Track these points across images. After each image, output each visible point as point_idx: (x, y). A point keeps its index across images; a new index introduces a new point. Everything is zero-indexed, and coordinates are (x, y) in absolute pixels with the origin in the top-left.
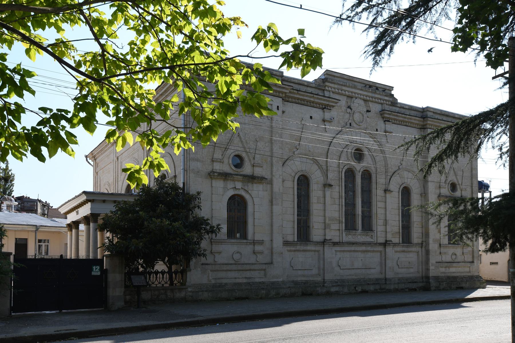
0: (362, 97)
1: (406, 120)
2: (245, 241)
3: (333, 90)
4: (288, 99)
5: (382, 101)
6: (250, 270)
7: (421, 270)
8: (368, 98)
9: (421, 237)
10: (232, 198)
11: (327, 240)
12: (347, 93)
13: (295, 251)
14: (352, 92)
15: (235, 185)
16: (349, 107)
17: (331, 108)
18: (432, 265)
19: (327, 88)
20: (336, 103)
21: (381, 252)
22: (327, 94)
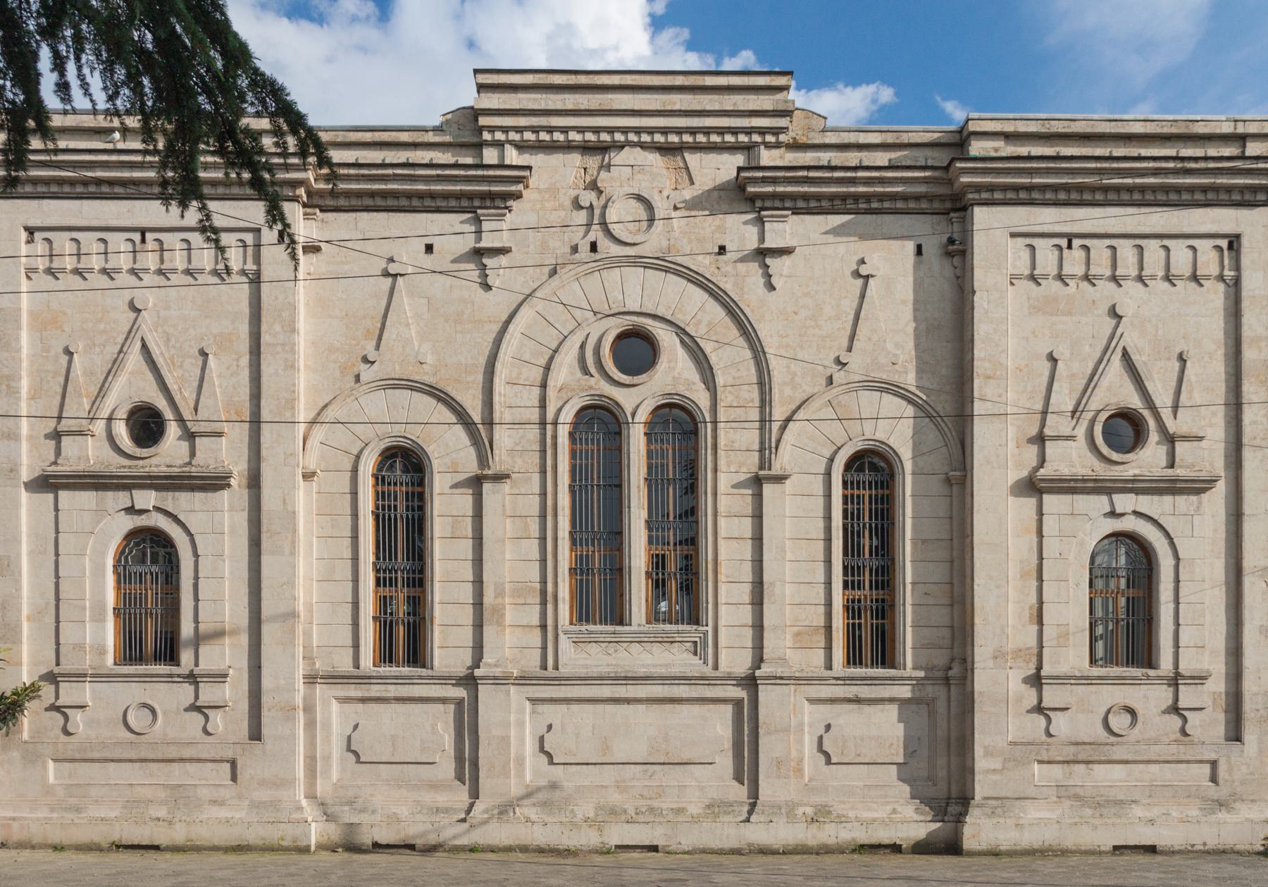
0: (645, 138)
1: (861, 189)
2: (423, 672)
3: (513, 136)
4: (1252, 198)
5: (743, 138)
6: (182, 760)
7: (942, 773)
8: (674, 138)
9: (947, 642)
10: (134, 536)
11: (1184, 677)
12: (574, 136)
13: (363, 700)
14: (596, 130)
15: (1112, 503)
16: (593, 186)
17: (510, 203)
18: (988, 753)
19: (487, 136)
20: (519, 180)
21: (738, 703)
22: (490, 156)
